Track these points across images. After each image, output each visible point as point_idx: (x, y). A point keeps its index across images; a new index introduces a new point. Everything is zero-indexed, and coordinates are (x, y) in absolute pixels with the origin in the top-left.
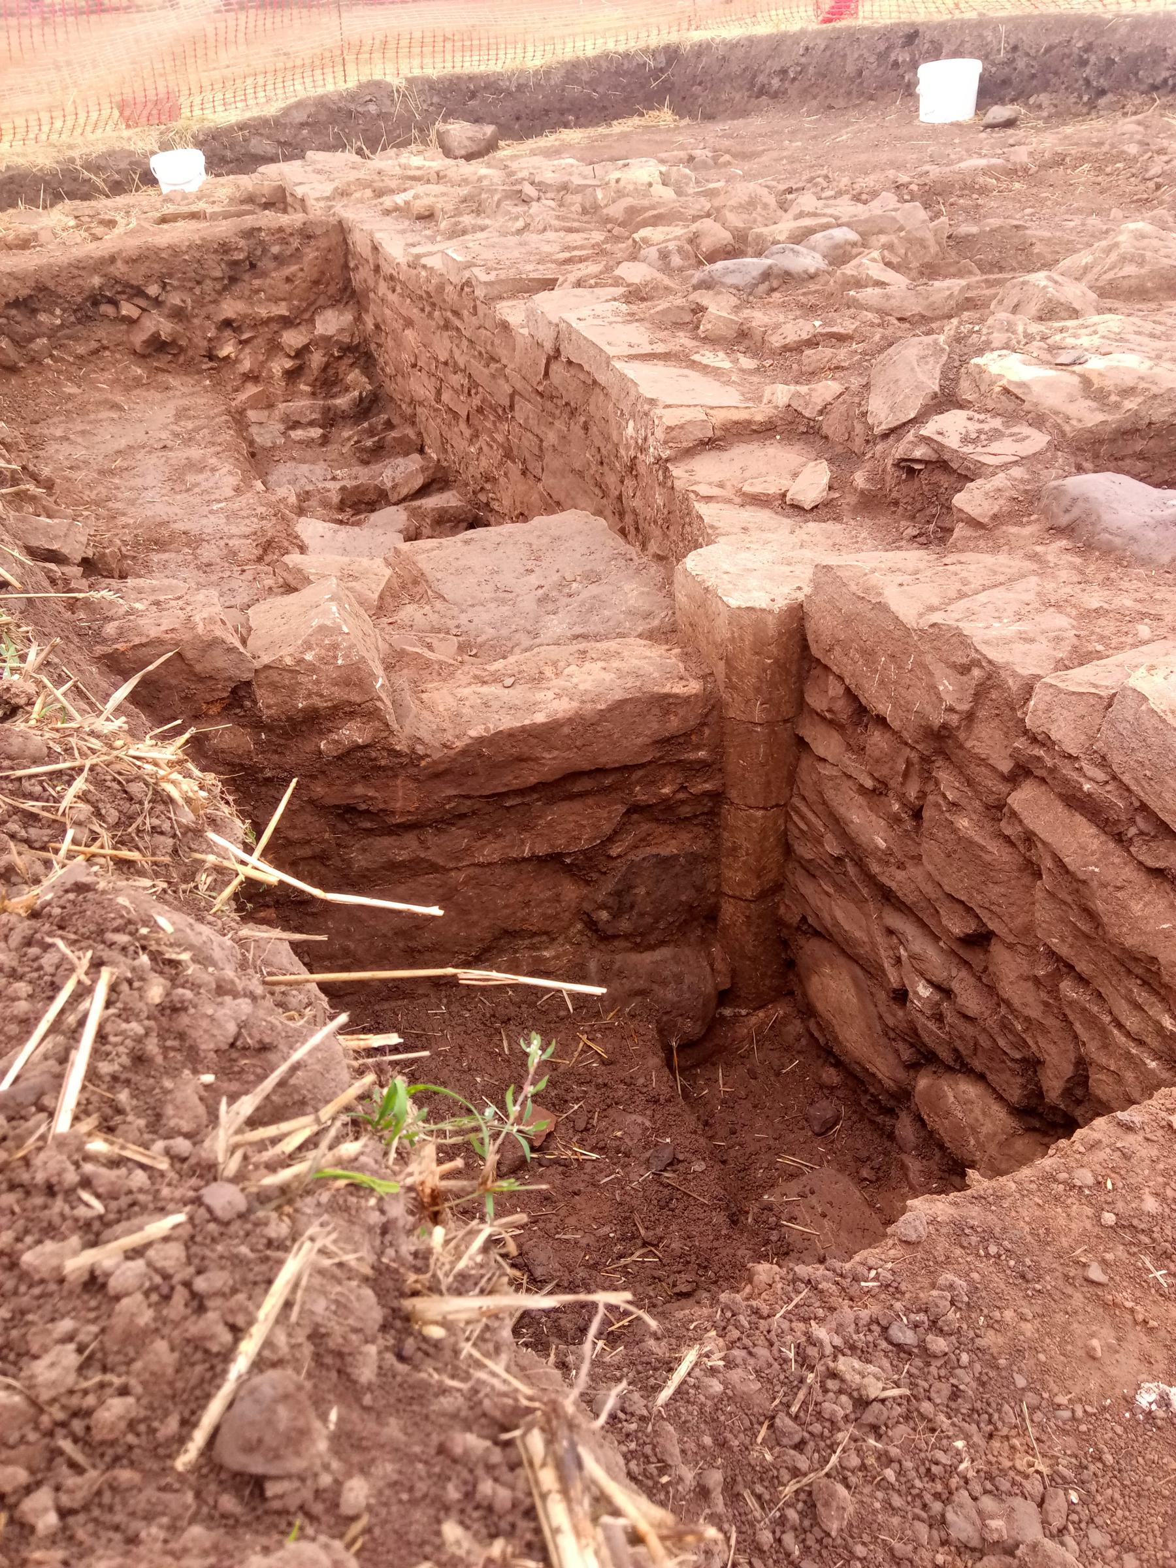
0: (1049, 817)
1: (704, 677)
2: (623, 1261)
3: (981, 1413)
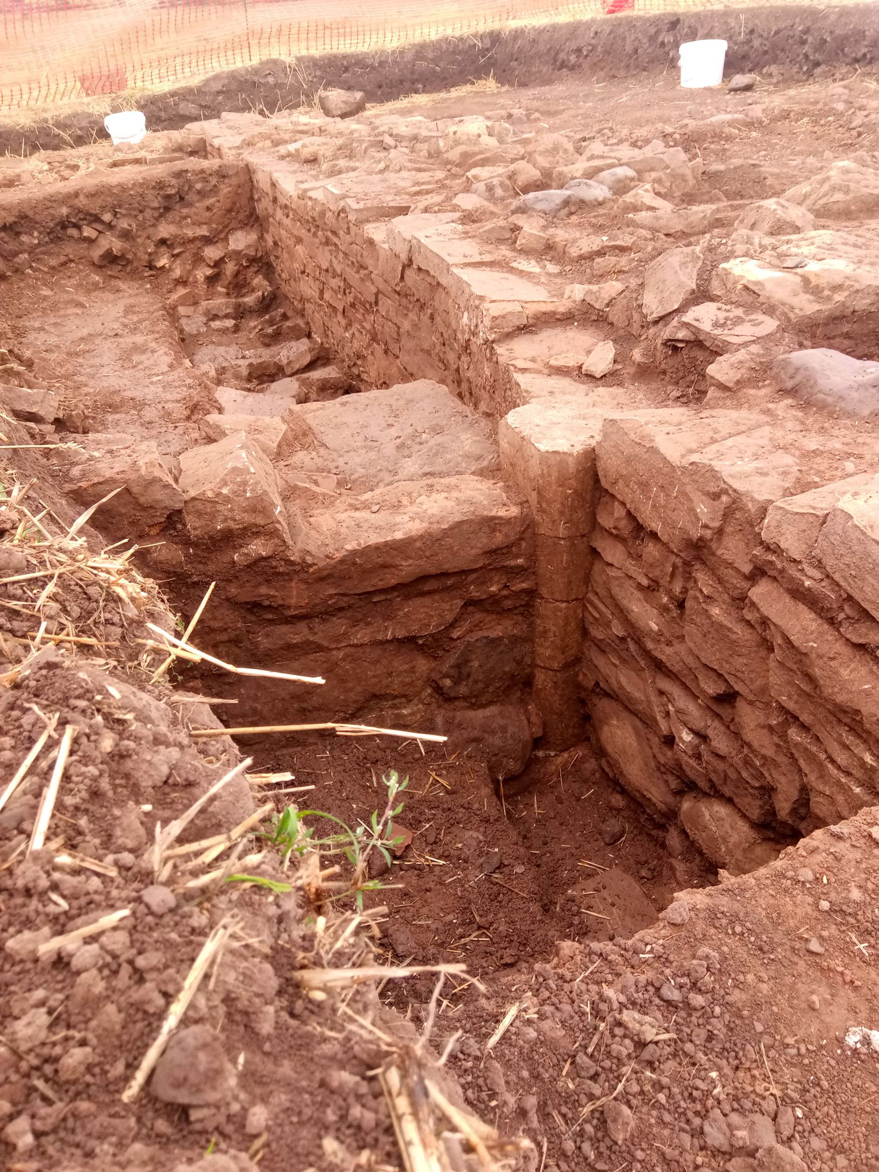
0: (779, 606)
1: (521, 504)
2: (463, 941)
3: (730, 1053)
